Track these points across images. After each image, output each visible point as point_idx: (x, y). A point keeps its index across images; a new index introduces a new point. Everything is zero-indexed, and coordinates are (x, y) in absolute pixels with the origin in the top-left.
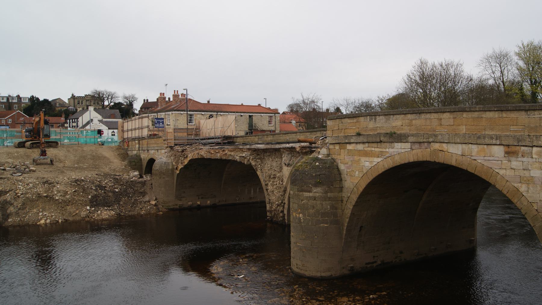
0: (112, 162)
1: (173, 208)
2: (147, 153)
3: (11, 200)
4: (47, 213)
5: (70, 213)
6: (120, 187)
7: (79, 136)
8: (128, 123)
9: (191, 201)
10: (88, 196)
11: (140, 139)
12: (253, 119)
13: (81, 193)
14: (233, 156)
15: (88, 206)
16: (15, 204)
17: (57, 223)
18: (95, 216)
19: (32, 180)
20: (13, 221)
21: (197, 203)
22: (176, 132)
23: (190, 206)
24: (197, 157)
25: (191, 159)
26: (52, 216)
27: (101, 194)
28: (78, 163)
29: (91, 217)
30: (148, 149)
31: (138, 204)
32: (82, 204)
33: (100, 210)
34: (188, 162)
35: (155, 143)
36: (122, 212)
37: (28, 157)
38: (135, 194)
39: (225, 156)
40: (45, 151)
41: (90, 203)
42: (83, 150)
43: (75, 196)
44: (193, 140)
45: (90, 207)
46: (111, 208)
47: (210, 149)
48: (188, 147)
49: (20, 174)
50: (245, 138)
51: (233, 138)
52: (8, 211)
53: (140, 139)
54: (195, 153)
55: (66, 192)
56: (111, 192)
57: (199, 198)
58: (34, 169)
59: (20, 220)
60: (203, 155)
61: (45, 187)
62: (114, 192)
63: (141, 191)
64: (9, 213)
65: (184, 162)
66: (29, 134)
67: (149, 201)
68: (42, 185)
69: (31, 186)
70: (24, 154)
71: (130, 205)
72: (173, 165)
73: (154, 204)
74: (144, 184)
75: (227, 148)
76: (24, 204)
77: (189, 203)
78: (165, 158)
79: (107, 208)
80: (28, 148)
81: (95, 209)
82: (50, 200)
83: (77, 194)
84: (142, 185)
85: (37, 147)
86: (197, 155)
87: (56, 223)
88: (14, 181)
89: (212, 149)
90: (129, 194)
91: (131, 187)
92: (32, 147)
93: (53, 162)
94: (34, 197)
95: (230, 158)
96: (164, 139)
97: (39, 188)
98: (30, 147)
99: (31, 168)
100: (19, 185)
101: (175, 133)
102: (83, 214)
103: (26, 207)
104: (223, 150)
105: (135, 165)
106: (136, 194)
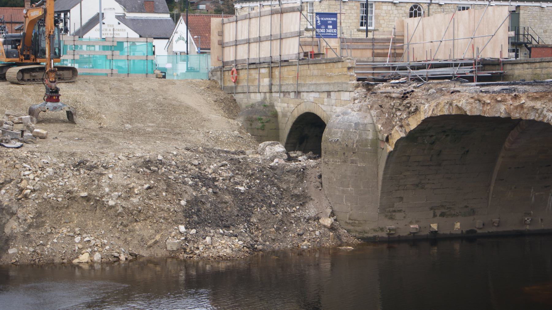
0: (209, 120)
1: (375, 237)
2: (297, 100)
3: (10, 205)
4: (93, 238)
5: (142, 238)
6: (248, 181)
7: (113, 55)
8: (236, 25)
9: (417, 222)
10: (180, 200)
11: (273, 65)
12: (521, 16)
13: (164, 194)
14: (539, 112)
15: (182, 224)
16: (20, 214)
17: (116, 264)
18: (201, 249)
19: (48, 159)
20: (18, 253)
21: (430, 226)
22: (346, 47)
23: (414, 233)
24: (446, 113)
25: (431, 117)
26: (103, 245)
27: (207, 198)
28: (130, 121)
29: (191, 250)
30: (300, 89)
31: (291, 223)
32: (167, 219)
33: (210, 236)
34: (419, 123)
35: (321, 75)
36: (257, 241)
37: (16, 102)
38: (281, 199)
39: (519, 109)
40: (57, 91)
41: (186, 217)
42: (133, 90)
43: (150, 199)
44: (388, 68)
45: (186, 228)
46: (231, 231)
47: (481, 92)
48: (414, 87)
49: (19, 144)
50: (538, 65)
51: (503, 64)
52: (7, 231)
53: (273, 65)
54: (440, 101)
55: (130, 188)
56: (229, 194)
57: (435, 216)
58: (45, 132)
59: (34, 251)
60: (464, 107)
61: (81, 176)
62: (236, 193)
63: (296, 192)
64: (8, 234)
65: (408, 125)
66: (12, 48)
67: (317, 219)
68: (73, 170)
69: (51, 173)
70: (7, 95)
71: (275, 226)
72: (376, 131)
73: (329, 225)
74: (302, 174)
75: (525, 92)
76: (39, 214)
77: (412, 226)
78: (355, 113)
79: (224, 232)
80: (13, 83)
81: (197, 232)
82: (96, 207)
83: (154, 194)
84: (298, 176)
85: (32, 79)
86: (447, 107)
87: (115, 262)
88: (12, 159)
89: (486, 92)
90: (269, 197)
91: (272, 181)
92: (21, 80)
93: (74, 117)
94: (60, 199)
95: (532, 116)
96: (350, 65)
97: (69, 178)
98: (18, 80)
99: (35, 130)
100: (25, 169)
101: (345, 51)
102: (173, 243)
103: (44, 223)
104: (513, 94)
105: (263, 129)
106: (285, 200)
